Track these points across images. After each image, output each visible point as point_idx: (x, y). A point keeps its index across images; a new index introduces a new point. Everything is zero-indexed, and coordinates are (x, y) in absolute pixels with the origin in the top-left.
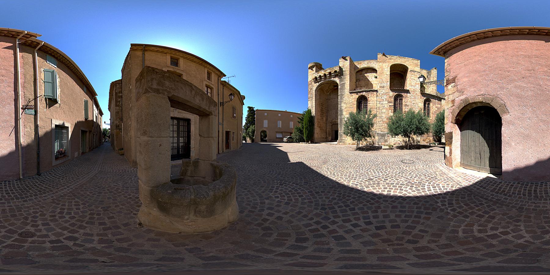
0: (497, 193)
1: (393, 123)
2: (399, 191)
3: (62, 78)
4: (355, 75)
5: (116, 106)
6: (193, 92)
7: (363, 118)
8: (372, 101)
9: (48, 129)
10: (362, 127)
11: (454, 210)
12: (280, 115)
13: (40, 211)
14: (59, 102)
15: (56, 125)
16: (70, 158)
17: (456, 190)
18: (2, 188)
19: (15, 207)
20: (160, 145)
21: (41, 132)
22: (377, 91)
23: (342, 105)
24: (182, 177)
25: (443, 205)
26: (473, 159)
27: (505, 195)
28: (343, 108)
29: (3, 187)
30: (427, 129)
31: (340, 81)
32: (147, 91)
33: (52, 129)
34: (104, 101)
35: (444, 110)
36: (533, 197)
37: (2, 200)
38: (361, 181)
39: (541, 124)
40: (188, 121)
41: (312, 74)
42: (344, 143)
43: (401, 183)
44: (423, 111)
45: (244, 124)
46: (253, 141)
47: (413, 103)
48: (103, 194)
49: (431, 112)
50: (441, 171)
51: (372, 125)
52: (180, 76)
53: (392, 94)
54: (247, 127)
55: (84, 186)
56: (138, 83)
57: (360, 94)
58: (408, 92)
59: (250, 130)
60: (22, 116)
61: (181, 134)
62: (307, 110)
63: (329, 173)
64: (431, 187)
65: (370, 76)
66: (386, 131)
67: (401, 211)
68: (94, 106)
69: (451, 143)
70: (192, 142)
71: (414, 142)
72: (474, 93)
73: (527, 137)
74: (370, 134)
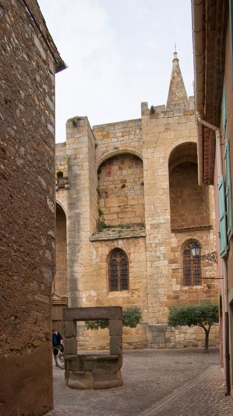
53: (176, 241)
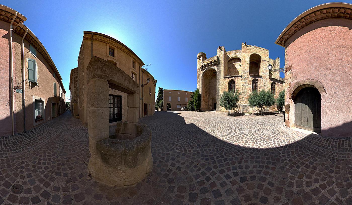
0: (318, 146)
1: (252, 99)
2: (255, 144)
3: (40, 66)
4: (227, 64)
5: (75, 87)
6: (124, 78)
7: (233, 95)
8: (239, 83)
9: (31, 102)
10: (231, 101)
11: (290, 160)
12: (179, 93)
13: (26, 161)
14: (38, 85)
15: (36, 100)
16: (45, 121)
17: (292, 144)
18: (2, 142)
19: (9, 158)
20: (103, 113)
21: (26, 104)
22: (241, 76)
23: (219, 86)
24: (116, 134)
25: (284, 156)
26: (303, 121)
27: (323, 147)
28: (219, 88)
29: (2, 141)
30: (273, 102)
31: (218, 69)
32: (94, 77)
33: (33, 102)
34: (66, 83)
35: (284, 90)
36: (341, 149)
37: (0, 151)
38: (231, 137)
39: (346, 99)
40: (120, 97)
41: (200, 63)
42: (220, 111)
43: (257, 138)
44: (271, 91)
45: (156, 99)
46: (162, 110)
47: (264, 85)
48: (66, 147)
49: (276, 91)
50: (282, 129)
51: (238, 100)
52: (115, 64)
53: (251, 79)
54: (158, 101)
55: (54, 140)
56: (88, 70)
57: (230, 79)
58: (261, 77)
59: (160, 103)
60: (14, 94)
61: (116, 106)
62: (196, 90)
63: (211, 131)
64: (276, 141)
65: (237, 65)
66: (247, 103)
67: (257, 162)
68: (60, 87)
69: (288, 111)
70: (123, 111)
71: (265, 111)
72: (304, 78)
73: (337, 107)
74: (237, 106)
